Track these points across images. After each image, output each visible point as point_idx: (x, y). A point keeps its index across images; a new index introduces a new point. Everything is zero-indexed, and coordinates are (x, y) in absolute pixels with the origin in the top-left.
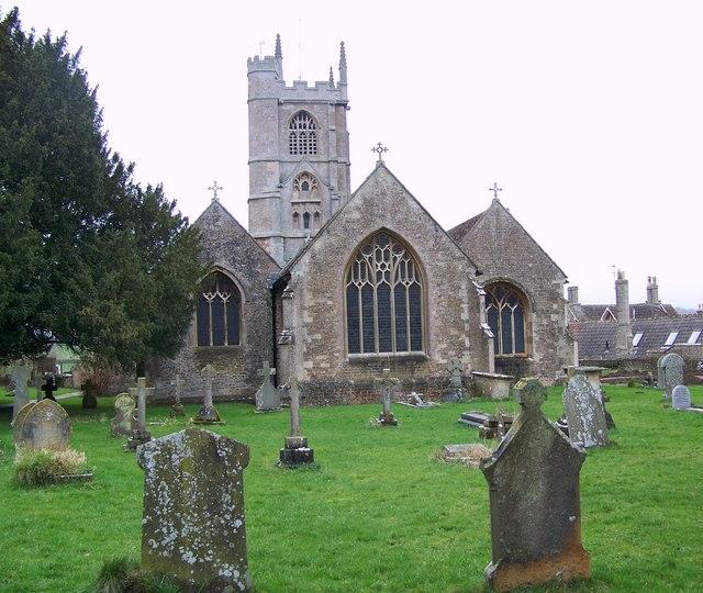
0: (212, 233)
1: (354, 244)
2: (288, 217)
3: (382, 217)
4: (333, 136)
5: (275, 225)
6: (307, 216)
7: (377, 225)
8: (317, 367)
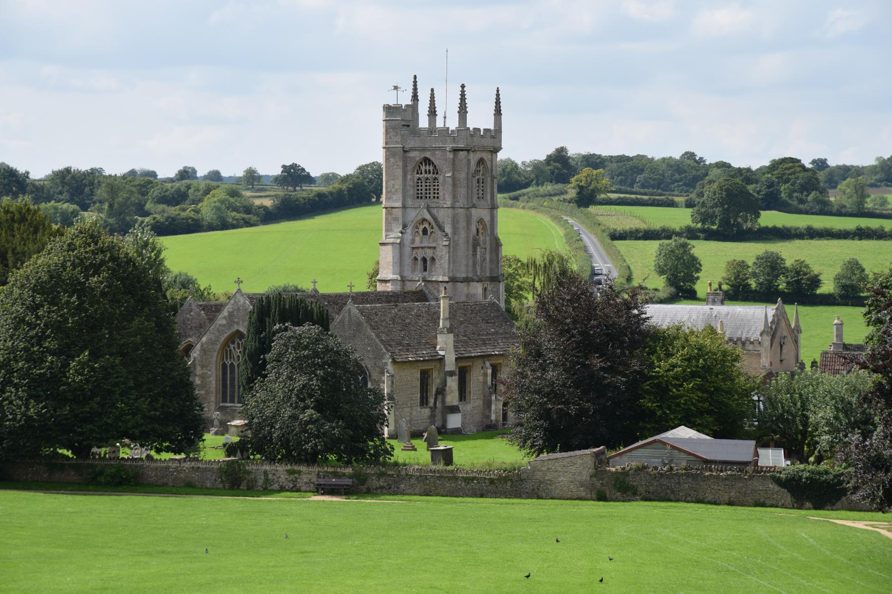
0: (188, 319)
1: (223, 338)
3: (238, 323)
6: (424, 260)
7: (235, 328)
8: (452, 392)
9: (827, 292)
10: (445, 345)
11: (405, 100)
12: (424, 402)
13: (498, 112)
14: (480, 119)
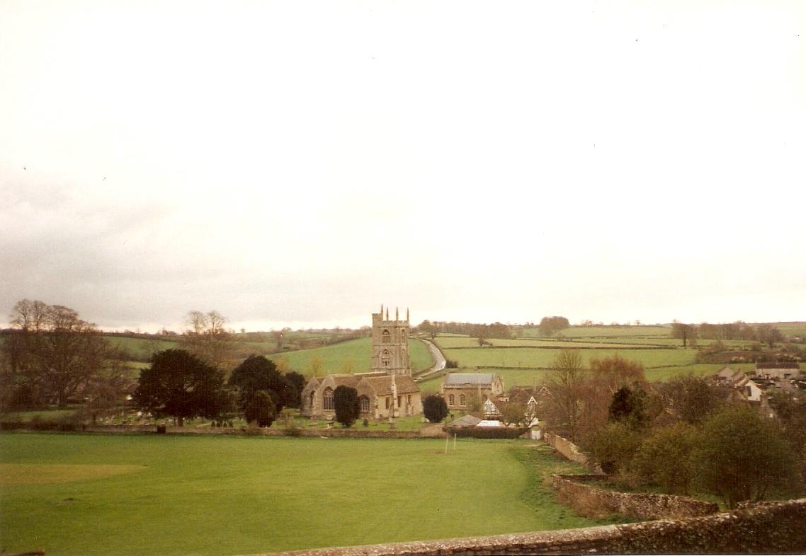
9: (755, 399)
10: (394, 388)
11: (379, 312)
12: (387, 407)
13: (408, 315)
14: (402, 318)
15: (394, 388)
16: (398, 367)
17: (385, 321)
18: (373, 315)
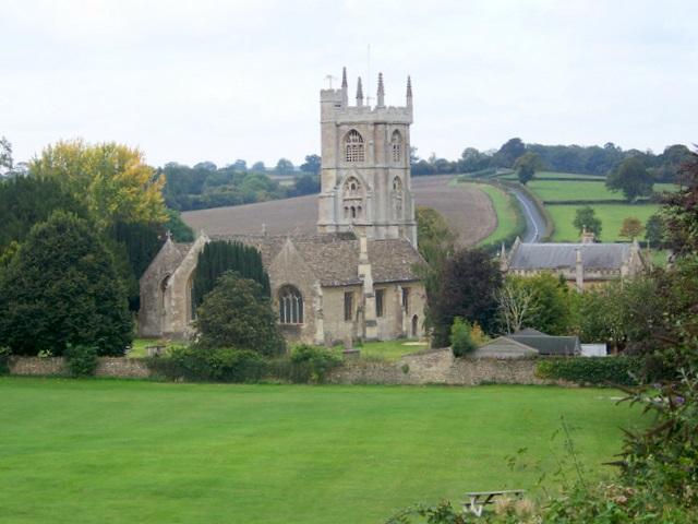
2: (341, 210)
4: (371, 148)
5: (332, 216)
6: (353, 208)
12: (347, 317)
13: (409, 94)
15: (365, 270)
16: (382, 220)
17: (353, 108)
18: (322, 92)
